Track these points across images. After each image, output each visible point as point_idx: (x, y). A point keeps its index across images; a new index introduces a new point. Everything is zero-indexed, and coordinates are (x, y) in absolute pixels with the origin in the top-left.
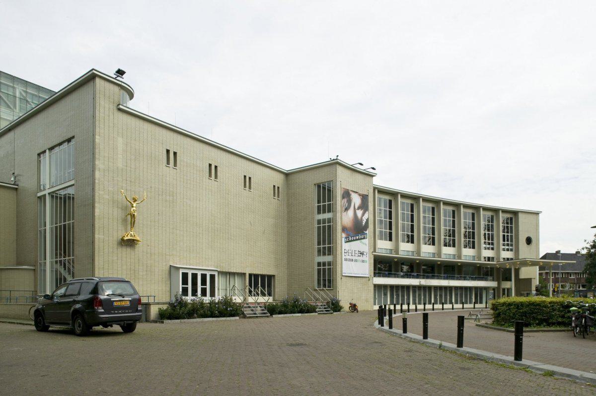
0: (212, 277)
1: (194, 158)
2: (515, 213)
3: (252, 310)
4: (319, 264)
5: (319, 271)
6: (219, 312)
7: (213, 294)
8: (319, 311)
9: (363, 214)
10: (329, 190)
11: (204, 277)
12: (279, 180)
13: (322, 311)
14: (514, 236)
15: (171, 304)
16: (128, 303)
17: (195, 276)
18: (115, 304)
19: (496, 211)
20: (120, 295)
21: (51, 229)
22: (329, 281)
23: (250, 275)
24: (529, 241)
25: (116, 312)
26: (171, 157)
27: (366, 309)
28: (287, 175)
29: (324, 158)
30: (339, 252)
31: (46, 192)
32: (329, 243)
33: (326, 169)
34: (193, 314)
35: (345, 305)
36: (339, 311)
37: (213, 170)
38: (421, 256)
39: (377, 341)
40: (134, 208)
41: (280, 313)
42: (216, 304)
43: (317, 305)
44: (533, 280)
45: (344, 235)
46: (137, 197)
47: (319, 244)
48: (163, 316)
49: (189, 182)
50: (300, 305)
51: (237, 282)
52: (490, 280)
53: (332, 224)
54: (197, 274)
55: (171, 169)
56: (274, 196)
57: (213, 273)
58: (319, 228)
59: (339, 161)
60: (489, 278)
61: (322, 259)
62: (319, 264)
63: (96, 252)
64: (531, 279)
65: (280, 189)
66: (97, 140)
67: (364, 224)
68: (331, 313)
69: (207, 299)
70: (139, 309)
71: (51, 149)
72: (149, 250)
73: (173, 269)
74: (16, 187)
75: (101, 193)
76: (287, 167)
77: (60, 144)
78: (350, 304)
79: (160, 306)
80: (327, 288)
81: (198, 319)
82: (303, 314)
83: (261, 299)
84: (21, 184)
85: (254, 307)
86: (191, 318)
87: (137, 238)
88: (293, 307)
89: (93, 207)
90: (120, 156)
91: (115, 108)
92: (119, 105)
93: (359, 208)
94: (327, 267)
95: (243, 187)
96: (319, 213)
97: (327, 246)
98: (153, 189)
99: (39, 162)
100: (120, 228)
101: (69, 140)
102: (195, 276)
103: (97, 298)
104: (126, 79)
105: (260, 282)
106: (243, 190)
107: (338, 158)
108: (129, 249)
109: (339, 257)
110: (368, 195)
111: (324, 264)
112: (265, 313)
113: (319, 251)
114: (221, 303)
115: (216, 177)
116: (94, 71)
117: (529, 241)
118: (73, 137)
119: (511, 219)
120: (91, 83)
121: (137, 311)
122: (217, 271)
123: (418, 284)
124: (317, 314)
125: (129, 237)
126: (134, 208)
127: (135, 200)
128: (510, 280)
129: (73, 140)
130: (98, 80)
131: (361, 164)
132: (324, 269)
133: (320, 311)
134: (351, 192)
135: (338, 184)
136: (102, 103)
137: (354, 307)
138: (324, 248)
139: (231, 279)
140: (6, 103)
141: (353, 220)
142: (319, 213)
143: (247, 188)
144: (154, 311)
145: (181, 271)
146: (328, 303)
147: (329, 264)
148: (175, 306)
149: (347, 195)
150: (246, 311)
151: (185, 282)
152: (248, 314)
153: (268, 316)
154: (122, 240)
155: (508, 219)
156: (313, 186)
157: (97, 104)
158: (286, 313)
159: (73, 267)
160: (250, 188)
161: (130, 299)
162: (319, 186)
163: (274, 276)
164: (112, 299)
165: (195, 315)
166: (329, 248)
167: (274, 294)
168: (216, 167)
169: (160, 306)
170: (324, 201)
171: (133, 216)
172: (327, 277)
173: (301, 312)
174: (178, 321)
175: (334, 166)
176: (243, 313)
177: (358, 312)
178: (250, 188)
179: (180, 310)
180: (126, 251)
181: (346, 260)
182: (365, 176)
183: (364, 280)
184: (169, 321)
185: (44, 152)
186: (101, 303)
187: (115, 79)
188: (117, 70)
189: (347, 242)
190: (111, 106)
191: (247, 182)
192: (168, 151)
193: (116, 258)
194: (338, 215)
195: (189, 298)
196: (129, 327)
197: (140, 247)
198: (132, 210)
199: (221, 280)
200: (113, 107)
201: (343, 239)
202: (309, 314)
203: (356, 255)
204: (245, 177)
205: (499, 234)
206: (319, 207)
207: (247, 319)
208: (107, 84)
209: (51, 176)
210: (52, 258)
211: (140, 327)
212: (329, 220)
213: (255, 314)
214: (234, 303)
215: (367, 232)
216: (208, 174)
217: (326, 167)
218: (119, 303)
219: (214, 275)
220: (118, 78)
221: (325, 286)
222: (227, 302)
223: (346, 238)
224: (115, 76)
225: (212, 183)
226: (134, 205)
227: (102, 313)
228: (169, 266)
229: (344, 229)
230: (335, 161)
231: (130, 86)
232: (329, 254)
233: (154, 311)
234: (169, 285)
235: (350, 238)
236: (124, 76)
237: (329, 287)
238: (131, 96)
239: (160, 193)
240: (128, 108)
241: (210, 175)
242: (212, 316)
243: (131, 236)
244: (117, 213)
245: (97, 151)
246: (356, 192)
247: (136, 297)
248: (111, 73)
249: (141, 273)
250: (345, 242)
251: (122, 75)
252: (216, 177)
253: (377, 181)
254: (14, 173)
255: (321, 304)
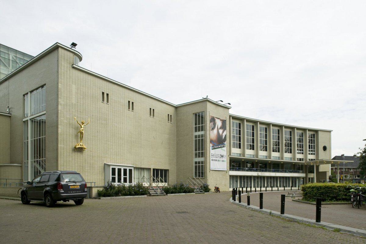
0: (130, 171)
1: (119, 98)
2: (317, 131)
3: (155, 191)
4: (196, 163)
5: (196, 167)
6: (134, 192)
7: (131, 181)
8: (196, 192)
9: (223, 132)
10: (202, 117)
11: (125, 171)
12: (171, 111)
13: (198, 192)
14: (315, 145)
15: (105, 188)
16: (79, 187)
17: (119, 170)
18: (71, 187)
19: (304, 130)
20: (74, 182)
21: (32, 141)
22: (202, 173)
23: (154, 170)
24: (325, 148)
25: (72, 192)
26: (105, 97)
27: (225, 191)
28: (176, 108)
29: (199, 98)
30: (208, 155)
31: (28, 118)
32: (202, 150)
33: (200, 104)
34: (119, 193)
35: (212, 188)
36: (208, 191)
37: (131, 105)
38: (259, 157)
39: (231, 210)
40: (82, 128)
41: (172, 193)
42: (133, 187)
43: (195, 188)
44: (327, 173)
45: (211, 145)
46: (84, 121)
47: (196, 150)
48: (100, 195)
49: (116, 112)
50: (184, 188)
51: (146, 174)
52: (301, 173)
53: (204, 138)
54: (121, 169)
55: (105, 104)
56: (168, 121)
57: (131, 168)
58: (196, 141)
59: (208, 99)
60: (301, 171)
61: (198, 159)
62: (196, 163)
63: (59, 155)
64: (326, 172)
65: (172, 116)
66: (60, 87)
67: (223, 138)
68: (203, 193)
69: (127, 184)
70: (85, 190)
71: (31, 92)
72: (91, 154)
73: (106, 166)
74: (10, 115)
75: (62, 119)
76: (176, 103)
77: (37, 89)
78: (215, 187)
79: (99, 189)
80: (201, 178)
81: (121, 197)
82: (186, 194)
83: (161, 184)
84: (13, 114)
85: (156, 189)
86: (117, 196)
87: (84, 147)
88: (180, 189)
89: (57, 128)
90: (74, 96)
91: (71, 67)
92: (73, 65)
93: (220, 128)
94: (201, 165)
95: (149, 115)
96: (196, 131)
97: (201, 151)
98: (94, 116)
99: (24, 100)
100: (74, 140)
101: (42, 87)
102: (119, 170)
103: (60, 184)
104: (77, 49)
105: (160, 174)
106: (149, 117)
107: (208, 97)
108: (79, 154)
109: (208, 158)
110: (226, 120)
111: (199, 163)
112: (162, 193)
113: (196, 155)
114: (136, 187)
115: (133, 109)
116: (58, 44)
117: (325, 148)
118: (45, 85)
119: (314, 135)
120: (56, 51)
121: (84, 191)
122: (133, 167)
123: (257, 175)
124: (194, 193)
125: (79, 146)
126: (82, 128)
127: (83, 124)
128: (313, 173)
129: (45, 86)
130: (60, 49)
131: (222, 101)
132: (199, 166)
133: (197, 192)
134: (215, 119)
135: (208, 113)
136: (63, 63)
137: (217, 189)
138: (199, 153)
139: (142, 172)
140: (4, 63)
141: (217, 136)
142: (196, 131)
143: (152, 116)
144: (95, 191)
145: (111, 167)
146: (201, 186)
147: (202, 163)
148: (107, 189)
149: (213, 120)
150: (151, 191)
151: (114, 173)
152: (152, 194)
153: (164, 195)
154: (75, 148)
155: (312, 135)
156: (192, 114)
157: (60, 64)
158: (176, 193)
159: (45, 164)
160: (153, 116)
161: (80, 184)
162: (196, 115)
163: (168, 170)
164: (69, 185)
165: (120, 194)
166: (202, 153)
167: (168, 181)
168: (133, 103)
169: (99, 189)
170: (199, 124)
171: (82, 133)
172: (201, 171)
173: (185, 192)
174: (109, 198)
175: (205, 102)
176: (149, 193)
177: (220, 192)
178: (153, 116)
179: (111, 191)
180: (77, 155)
181: (212, 160)
182: (224, 109)
183: (223, 172)
184: (104, 198)
185: (27, 94)
186: (62, 187)
187: (71, 48)
188: (72, 43)
189: (213, 149)
190: (68, 65)
191: (152, 112)
192: (103, 93)
193: (71, 159)
194: (208, 132)
195: (116, 184)
196: (79, 202)
197: (86, 152)
198: (81, 129)
199: (136, 173)
200: (69, 66)
201: (211, 147)
202: (189, 193)
203: (219, 157)
204: (150, 109)
205: (307, 144)
206: (196, 128)
207: (152, 197)
208: (66, 52)
209: (31, 109)
210: (32, 159)
211: (86, 201)
212: (202, 136)
213: (157, 193)
214: (144, 187)
215: (225, 143)
216: (128, 107)
217: (200, 103)
218: (73, 187)
219: (132, 169)
220: (73, 48)
221: (199, 176)
222: (139, 186)
223: (213, 147)
224: (70, 47)
225: (130, 113)
226: (83, 126)
227: (63, 193)
228: (104, 164)
229: (211, 141)
230: (206, 99)
231: (80, 53)
232: (202, 157)
233: (95, 191)
234: (104, 176)
235: (215, 147)
236: (76, 47)
237: (202, 177)
238: (81, 59)
239: (98, 119)
240: (79, 66)
241: (129, 108)
242: (130, 194)
243: (81, 145)
244: (72, 132)
245: (60, 93)
246: (219, 119)
247: (84, 183)
248: (68, 45)
249: (86, 168)
250: (212, 149)
251: (75, 46)
252: (133, 109)
253: (232, 112)
254: (8, 107)
255: (197, 187)
